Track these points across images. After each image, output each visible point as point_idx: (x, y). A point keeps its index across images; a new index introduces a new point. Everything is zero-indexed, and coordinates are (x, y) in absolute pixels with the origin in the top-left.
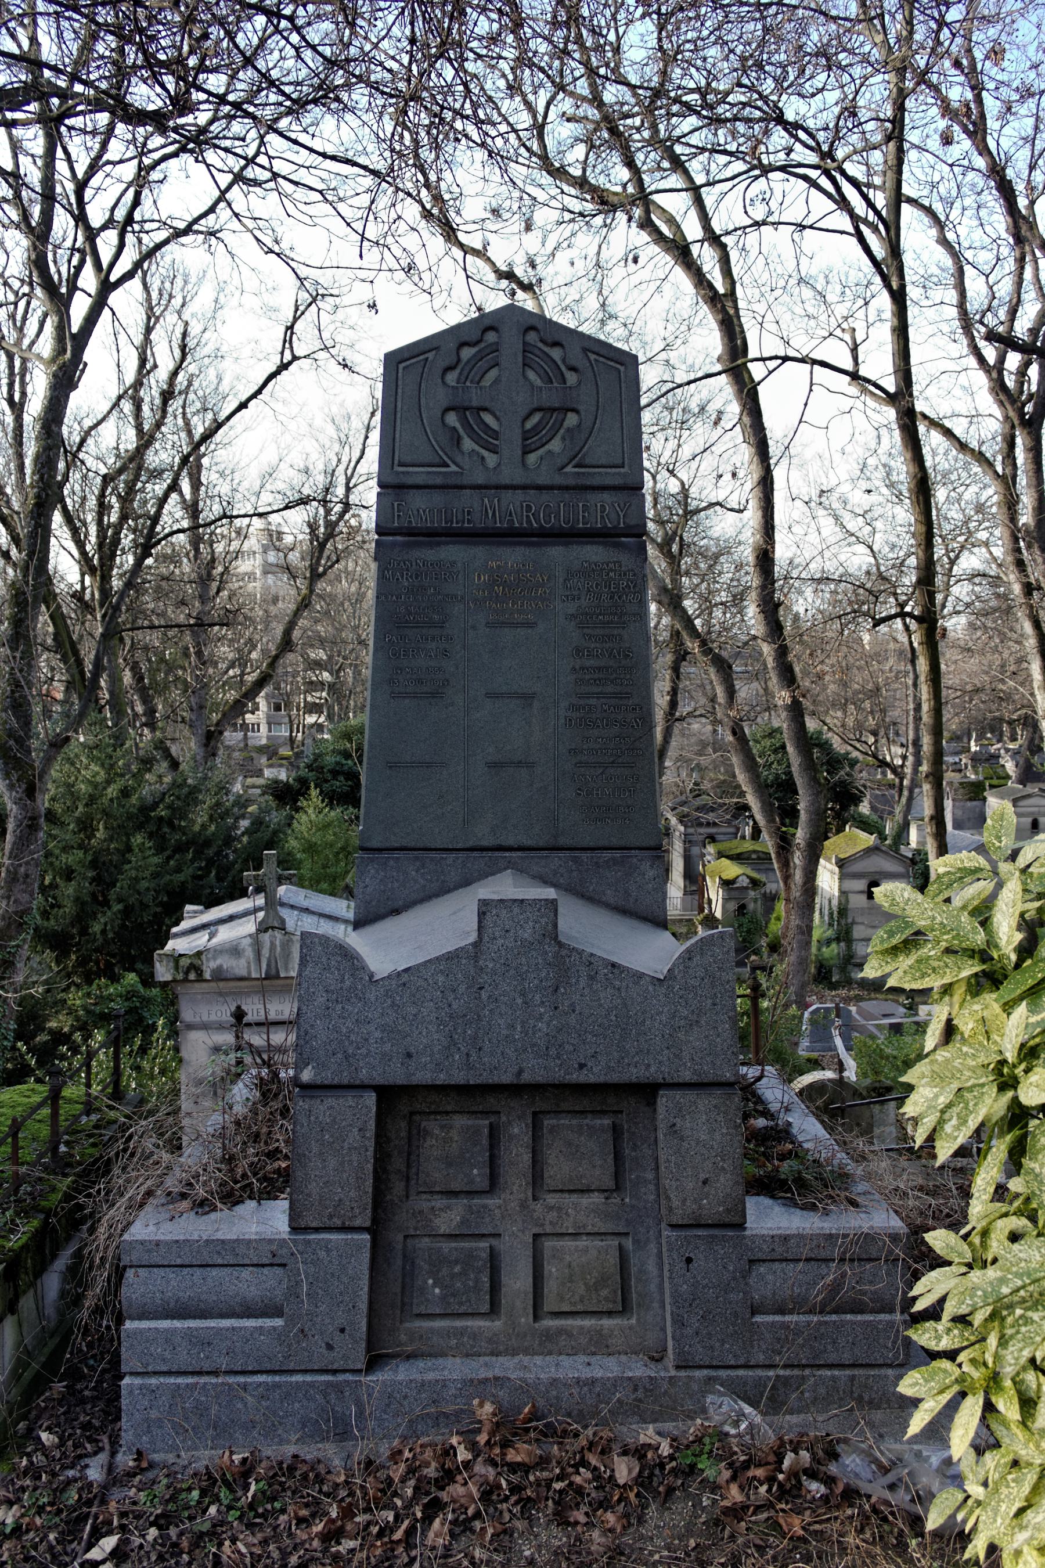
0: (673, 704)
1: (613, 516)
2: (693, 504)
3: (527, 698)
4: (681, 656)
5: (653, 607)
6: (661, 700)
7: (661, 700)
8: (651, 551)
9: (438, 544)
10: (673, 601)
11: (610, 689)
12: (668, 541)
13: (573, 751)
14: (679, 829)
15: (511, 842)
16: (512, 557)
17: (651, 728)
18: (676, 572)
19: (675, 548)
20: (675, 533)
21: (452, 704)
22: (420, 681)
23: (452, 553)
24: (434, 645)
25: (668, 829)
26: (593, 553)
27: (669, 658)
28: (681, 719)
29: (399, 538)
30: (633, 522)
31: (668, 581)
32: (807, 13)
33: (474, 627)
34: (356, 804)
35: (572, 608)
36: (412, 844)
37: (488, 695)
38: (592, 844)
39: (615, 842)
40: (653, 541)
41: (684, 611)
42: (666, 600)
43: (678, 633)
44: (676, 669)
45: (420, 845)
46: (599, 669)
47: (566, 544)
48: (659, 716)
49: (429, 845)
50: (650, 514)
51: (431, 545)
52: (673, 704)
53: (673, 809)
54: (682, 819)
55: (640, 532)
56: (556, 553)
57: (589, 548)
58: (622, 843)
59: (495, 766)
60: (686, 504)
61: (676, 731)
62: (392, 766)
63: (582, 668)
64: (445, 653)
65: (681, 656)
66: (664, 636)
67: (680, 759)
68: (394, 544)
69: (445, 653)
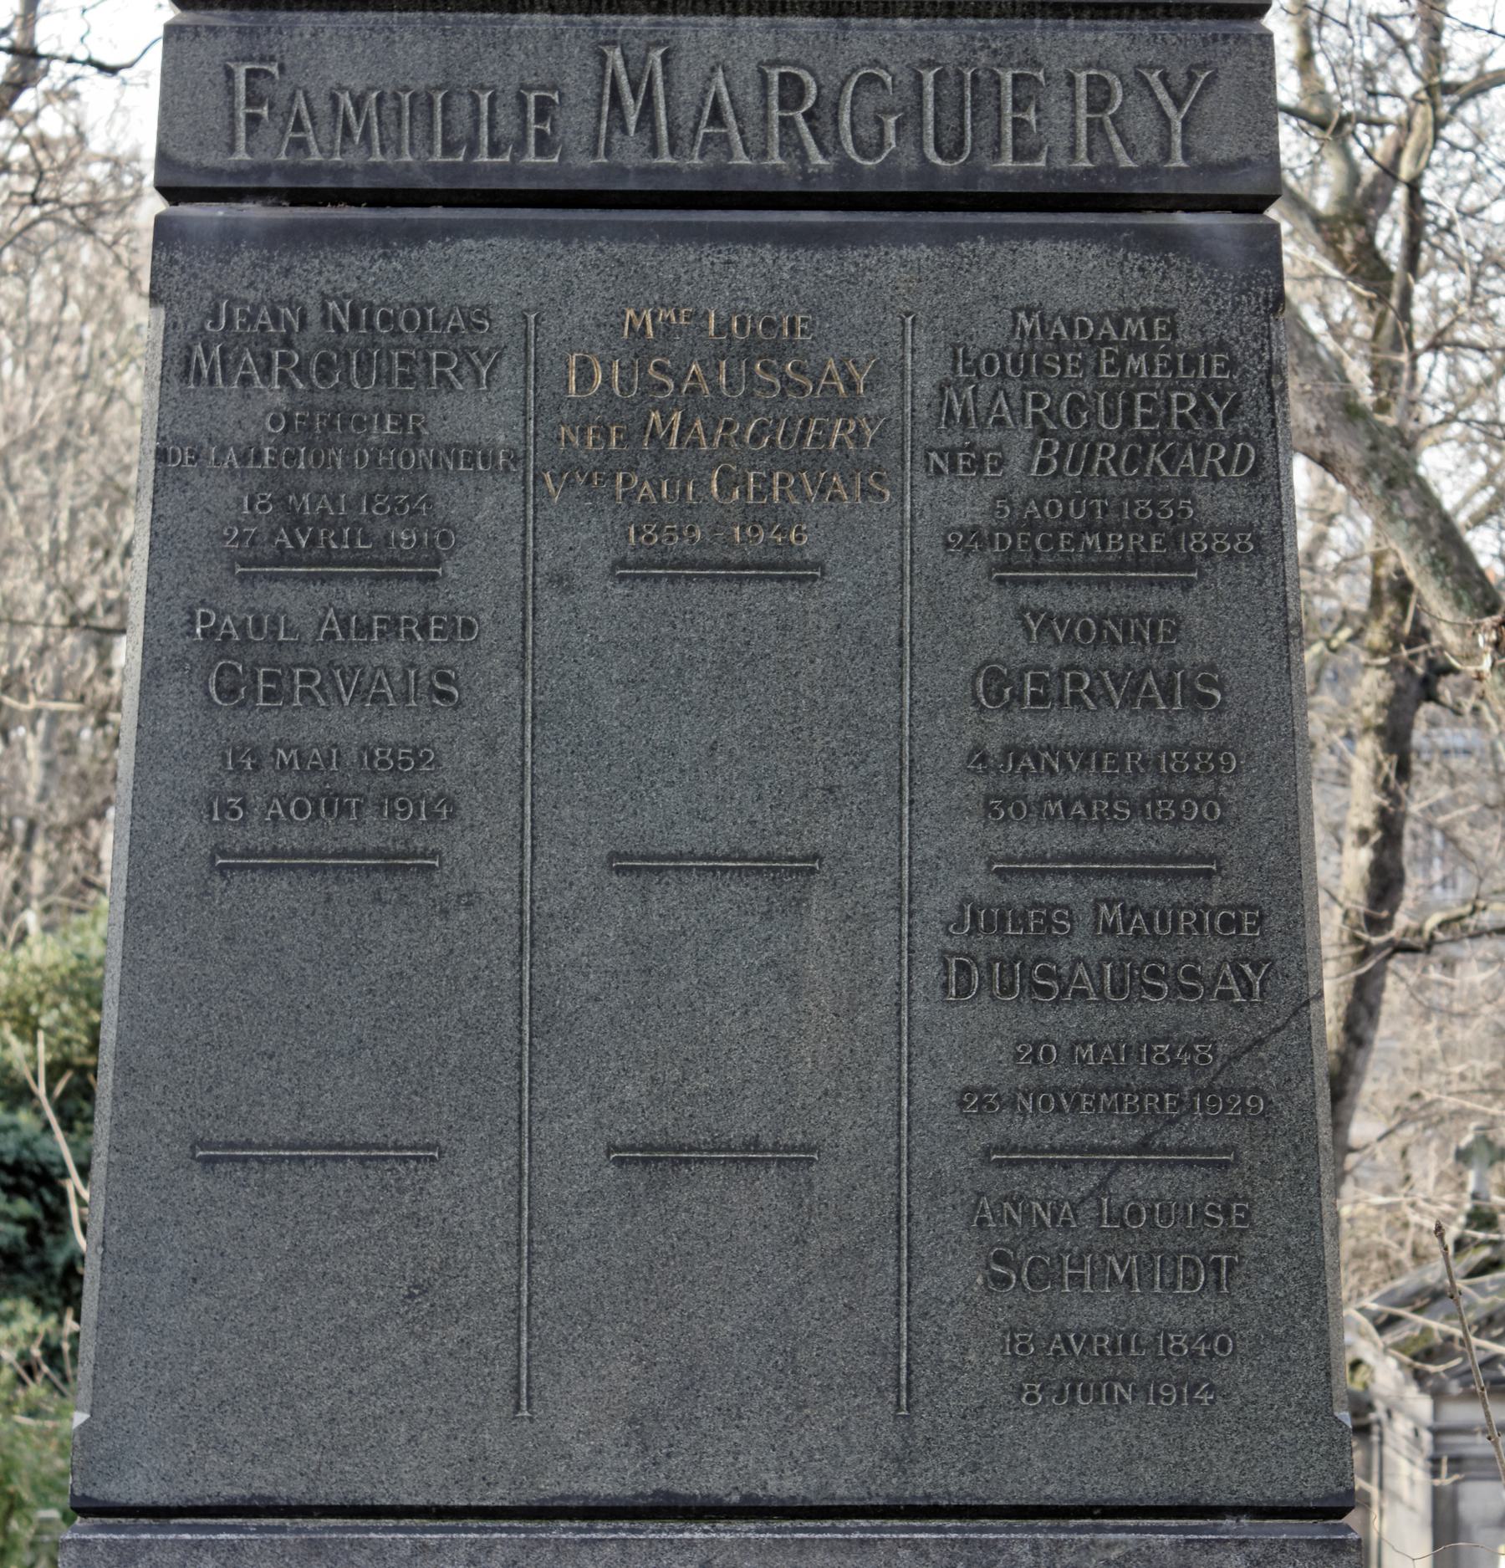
0: (1385, 883)
1: (1142, 123)
2: (1462, 55)
3: (789, 872)
4: (1421, 682)
5: (1303, 476)
6: (1342, 870)
7: (1342, 870)
8: (1299, 253)
9: (417, 235)
10: (1390, 472)
11: (1133, 837)
12: (1360, 207)
13: (978, 1101)
14: (1406, 1409)
15: (715, 1484)
16: (730, 279)
17: (1306, 1001)
18: (1393, 340)
19: (1390, 235)
20: (1389, 172)
21: (470, 898)
22: (335, 803)
23: (484, 269)
24: (393, 652)
25: (1362, 1405)
26: (1062, 272)
27: (1371, 687)
28: (1413, 947)
29: (253, 212)
30: (1226, 151)
31: (1358, 372)
32: (73, 69)
33: (562, 581)
34: (62, 1288)
35: (970, 503)
36: (296, 1490)
37: (621, 863)
38: (1055, 1492)
39: (1149, 1485)
40: (1300, 204)
41: (1426, 497)
42: (1353, 453)
43: (1403, 589)
44: (1395, 736)
45: (335, 1495)
46: (1085, 754)
47: (948, 238)
48: (1332, 929)
49: (364, 1493)
50: (1288, 89)
51: (381, 236)
52: (1385, 883)
53: (1386, 1324)
54: (1423, 1359)
55: (1253, 196)
56: (900, 268)
57: (1041, 251)
58: (1183, 1490)
59: (653, 1159)
60: (1436, 56)
61: (1394, 996)
62: (211, 1157)
63: (1014, 752)
64: (442, 689)
65: (1421, 682)
66: (1353, 593)
67: (1413, 1111)
68: (231, 238)
69: (442, 689)
